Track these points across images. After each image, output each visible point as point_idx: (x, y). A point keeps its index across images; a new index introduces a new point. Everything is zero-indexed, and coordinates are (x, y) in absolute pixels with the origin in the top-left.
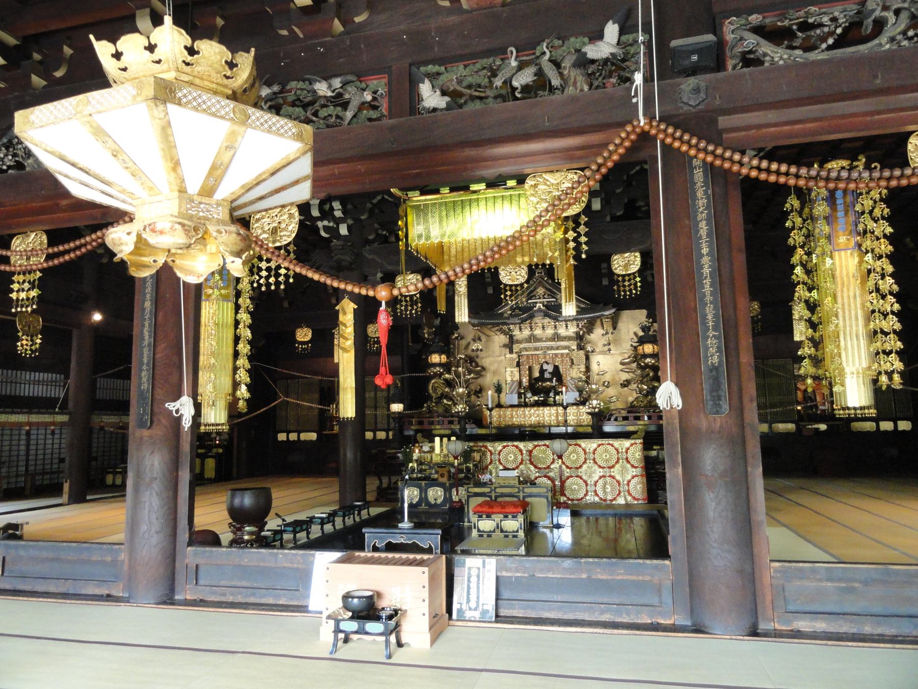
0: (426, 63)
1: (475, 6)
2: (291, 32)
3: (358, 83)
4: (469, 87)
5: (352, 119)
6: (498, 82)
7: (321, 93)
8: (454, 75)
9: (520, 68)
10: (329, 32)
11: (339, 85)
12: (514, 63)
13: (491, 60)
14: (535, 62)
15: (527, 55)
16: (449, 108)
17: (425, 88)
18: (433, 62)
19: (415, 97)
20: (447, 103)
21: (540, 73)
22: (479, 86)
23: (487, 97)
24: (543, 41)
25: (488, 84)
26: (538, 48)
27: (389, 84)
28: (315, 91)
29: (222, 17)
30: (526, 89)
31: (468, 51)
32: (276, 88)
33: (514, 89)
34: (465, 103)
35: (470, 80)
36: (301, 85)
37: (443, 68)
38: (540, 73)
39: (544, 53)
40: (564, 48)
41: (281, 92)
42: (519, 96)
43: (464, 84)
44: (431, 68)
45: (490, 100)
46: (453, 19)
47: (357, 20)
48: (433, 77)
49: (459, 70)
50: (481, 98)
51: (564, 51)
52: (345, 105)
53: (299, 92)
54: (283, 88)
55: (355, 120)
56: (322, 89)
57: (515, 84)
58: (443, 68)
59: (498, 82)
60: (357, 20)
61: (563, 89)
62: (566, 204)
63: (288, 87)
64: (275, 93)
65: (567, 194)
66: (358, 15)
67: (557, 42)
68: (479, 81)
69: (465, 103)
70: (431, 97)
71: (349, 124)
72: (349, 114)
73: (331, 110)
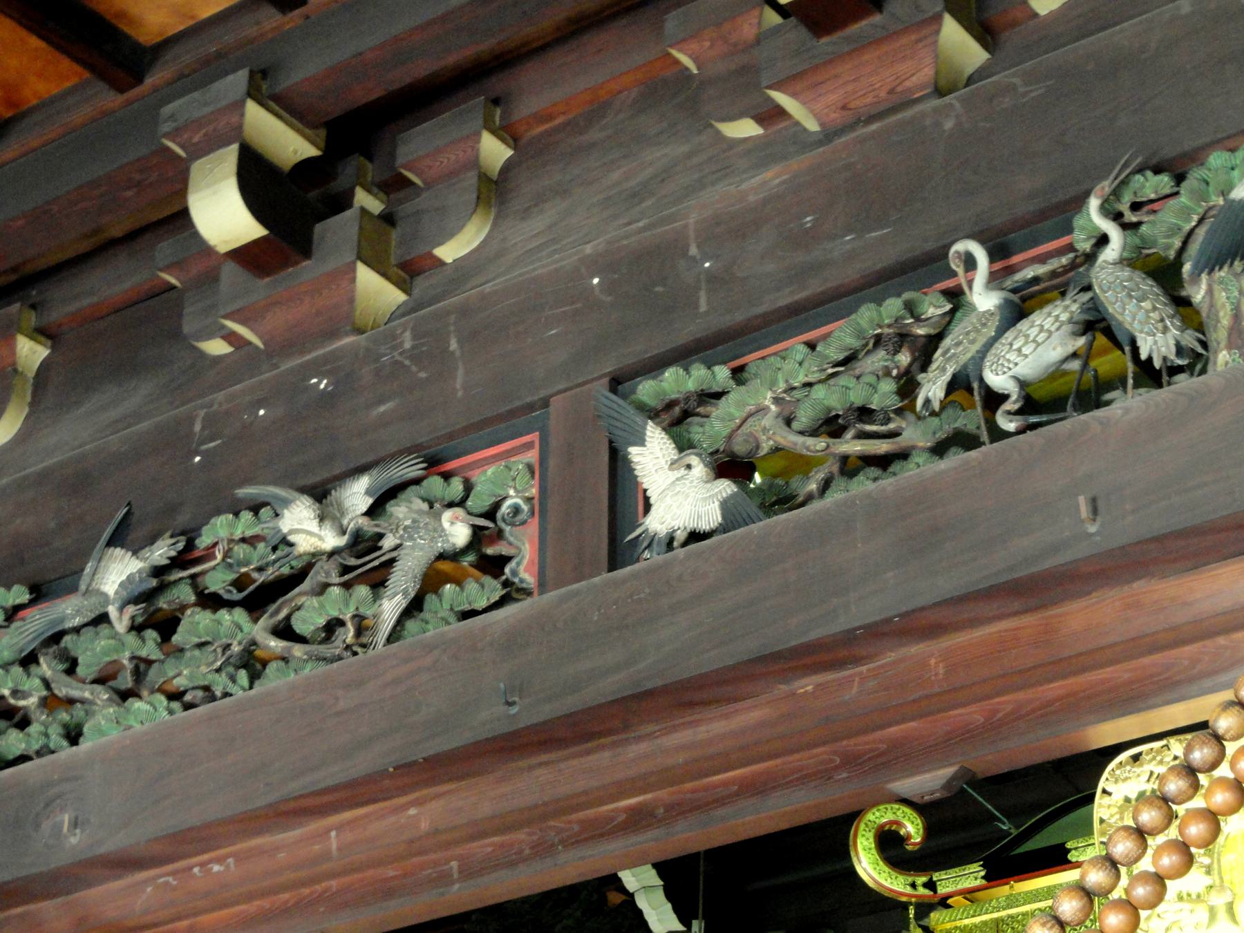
0: (654, 367)
1: (836, 116)
2: (231, 337)
3: (435, 483)
4: (832, 426)
5: (400, 622)
6: (933, 388)
7: (304, 544)
8: (765, 401)
9: (1018, 309)
10: (343, 319)
11: (364, 503)
12: (985, 300)
13: (893, 306)
14: (1073, 276)
15: (1041, 259)
16: (732, 518)
17: (652, 457)
18: (682, 356)
19: (623, 495)
20: (725, 505)
21: (1096, 324)
22: (865, 413)
23: (903, 455)
24: (1087, 194)
25: (894, 402)
26: (1078, 222)
27: (539, 471)
28: (286, 542)
29: (42, 333)
30: (1040, 403)
31: (814, 287)
32: (161, 552)
33: (994, 400)
34: (826, 485)
35: (829, 398)
36: (245, 524)
37: (722, 373)
38: (1096, 324)
39: (1103, 240)
40: (1183, 199)
41: (180, 561)
42: (1010, 426)
43: (805, 417)
44: (675, 382)
45: (918, 458)
46: (772, 177)
47: (449, 252)
48: (678, 418)
49: (789, 365)
50: (883, 462)
51: (1185, 213)
52: (378, 581)
53: (241, 551)
54: (190, 546)
55: (411, 625)
56: (305, 528)
57: (997, 380)
58: (722, 373)
59: (933, 388)
60: (449, 252)
61: (1195, 360)
62: (1145, 877)
63: (204, 541)
64: (158, 571)
65: (1141, 834)
66: (446, 235)
67: (1152, 185)
68: (857, 396)
69: (826, 485)
70: (678, 493)
71: (391, 639)
72: (390, 607)
73: (335, 603)
